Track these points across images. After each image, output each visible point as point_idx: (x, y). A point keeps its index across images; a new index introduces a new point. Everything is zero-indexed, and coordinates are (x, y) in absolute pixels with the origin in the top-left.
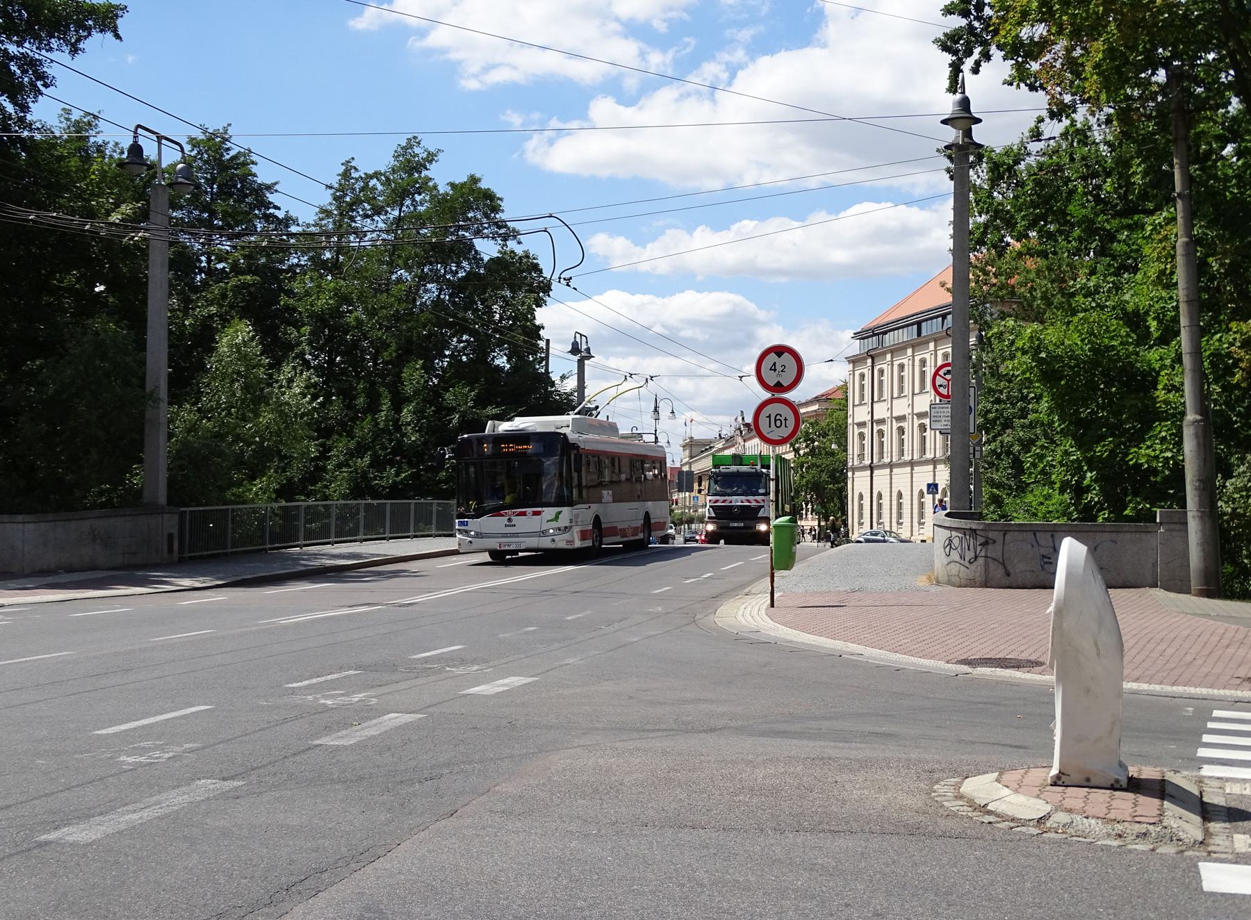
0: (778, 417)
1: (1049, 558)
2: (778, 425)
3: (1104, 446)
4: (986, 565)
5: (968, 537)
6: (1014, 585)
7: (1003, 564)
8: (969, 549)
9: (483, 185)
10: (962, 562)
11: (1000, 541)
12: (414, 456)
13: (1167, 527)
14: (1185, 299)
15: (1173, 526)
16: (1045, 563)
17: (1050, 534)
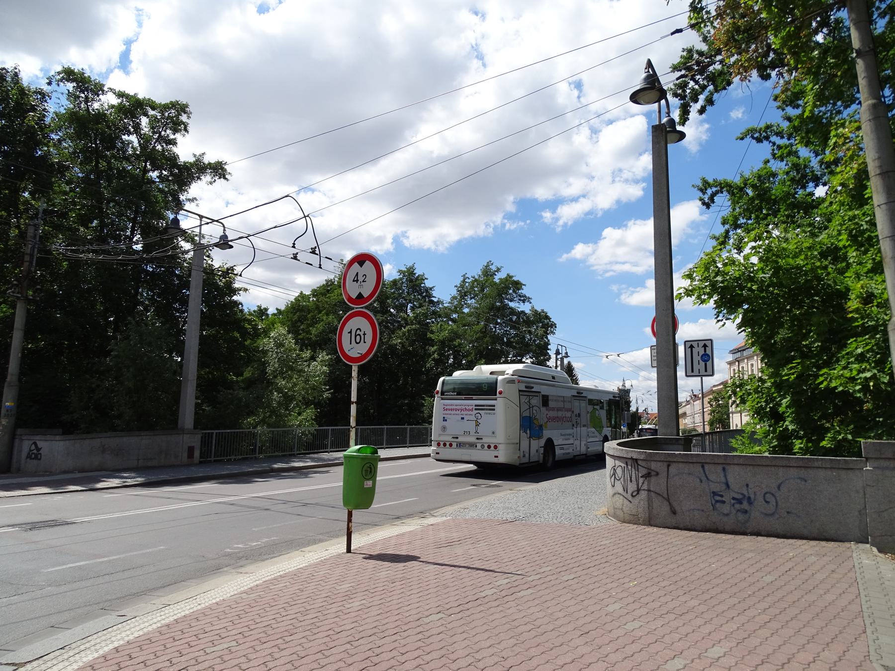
0: (358, 332)
1: (722, 496)
2: (358, 341)
3: (791, 368)
4: (650, 500)
5: (630, 467)
6: (681, 526)
7: (668, 500)
9: (515, 279)
10: (625, 494)
11: (663, 474)
13: (876, 464)
14: (878, 172)
15: (885, 463)
16: (717, 501)
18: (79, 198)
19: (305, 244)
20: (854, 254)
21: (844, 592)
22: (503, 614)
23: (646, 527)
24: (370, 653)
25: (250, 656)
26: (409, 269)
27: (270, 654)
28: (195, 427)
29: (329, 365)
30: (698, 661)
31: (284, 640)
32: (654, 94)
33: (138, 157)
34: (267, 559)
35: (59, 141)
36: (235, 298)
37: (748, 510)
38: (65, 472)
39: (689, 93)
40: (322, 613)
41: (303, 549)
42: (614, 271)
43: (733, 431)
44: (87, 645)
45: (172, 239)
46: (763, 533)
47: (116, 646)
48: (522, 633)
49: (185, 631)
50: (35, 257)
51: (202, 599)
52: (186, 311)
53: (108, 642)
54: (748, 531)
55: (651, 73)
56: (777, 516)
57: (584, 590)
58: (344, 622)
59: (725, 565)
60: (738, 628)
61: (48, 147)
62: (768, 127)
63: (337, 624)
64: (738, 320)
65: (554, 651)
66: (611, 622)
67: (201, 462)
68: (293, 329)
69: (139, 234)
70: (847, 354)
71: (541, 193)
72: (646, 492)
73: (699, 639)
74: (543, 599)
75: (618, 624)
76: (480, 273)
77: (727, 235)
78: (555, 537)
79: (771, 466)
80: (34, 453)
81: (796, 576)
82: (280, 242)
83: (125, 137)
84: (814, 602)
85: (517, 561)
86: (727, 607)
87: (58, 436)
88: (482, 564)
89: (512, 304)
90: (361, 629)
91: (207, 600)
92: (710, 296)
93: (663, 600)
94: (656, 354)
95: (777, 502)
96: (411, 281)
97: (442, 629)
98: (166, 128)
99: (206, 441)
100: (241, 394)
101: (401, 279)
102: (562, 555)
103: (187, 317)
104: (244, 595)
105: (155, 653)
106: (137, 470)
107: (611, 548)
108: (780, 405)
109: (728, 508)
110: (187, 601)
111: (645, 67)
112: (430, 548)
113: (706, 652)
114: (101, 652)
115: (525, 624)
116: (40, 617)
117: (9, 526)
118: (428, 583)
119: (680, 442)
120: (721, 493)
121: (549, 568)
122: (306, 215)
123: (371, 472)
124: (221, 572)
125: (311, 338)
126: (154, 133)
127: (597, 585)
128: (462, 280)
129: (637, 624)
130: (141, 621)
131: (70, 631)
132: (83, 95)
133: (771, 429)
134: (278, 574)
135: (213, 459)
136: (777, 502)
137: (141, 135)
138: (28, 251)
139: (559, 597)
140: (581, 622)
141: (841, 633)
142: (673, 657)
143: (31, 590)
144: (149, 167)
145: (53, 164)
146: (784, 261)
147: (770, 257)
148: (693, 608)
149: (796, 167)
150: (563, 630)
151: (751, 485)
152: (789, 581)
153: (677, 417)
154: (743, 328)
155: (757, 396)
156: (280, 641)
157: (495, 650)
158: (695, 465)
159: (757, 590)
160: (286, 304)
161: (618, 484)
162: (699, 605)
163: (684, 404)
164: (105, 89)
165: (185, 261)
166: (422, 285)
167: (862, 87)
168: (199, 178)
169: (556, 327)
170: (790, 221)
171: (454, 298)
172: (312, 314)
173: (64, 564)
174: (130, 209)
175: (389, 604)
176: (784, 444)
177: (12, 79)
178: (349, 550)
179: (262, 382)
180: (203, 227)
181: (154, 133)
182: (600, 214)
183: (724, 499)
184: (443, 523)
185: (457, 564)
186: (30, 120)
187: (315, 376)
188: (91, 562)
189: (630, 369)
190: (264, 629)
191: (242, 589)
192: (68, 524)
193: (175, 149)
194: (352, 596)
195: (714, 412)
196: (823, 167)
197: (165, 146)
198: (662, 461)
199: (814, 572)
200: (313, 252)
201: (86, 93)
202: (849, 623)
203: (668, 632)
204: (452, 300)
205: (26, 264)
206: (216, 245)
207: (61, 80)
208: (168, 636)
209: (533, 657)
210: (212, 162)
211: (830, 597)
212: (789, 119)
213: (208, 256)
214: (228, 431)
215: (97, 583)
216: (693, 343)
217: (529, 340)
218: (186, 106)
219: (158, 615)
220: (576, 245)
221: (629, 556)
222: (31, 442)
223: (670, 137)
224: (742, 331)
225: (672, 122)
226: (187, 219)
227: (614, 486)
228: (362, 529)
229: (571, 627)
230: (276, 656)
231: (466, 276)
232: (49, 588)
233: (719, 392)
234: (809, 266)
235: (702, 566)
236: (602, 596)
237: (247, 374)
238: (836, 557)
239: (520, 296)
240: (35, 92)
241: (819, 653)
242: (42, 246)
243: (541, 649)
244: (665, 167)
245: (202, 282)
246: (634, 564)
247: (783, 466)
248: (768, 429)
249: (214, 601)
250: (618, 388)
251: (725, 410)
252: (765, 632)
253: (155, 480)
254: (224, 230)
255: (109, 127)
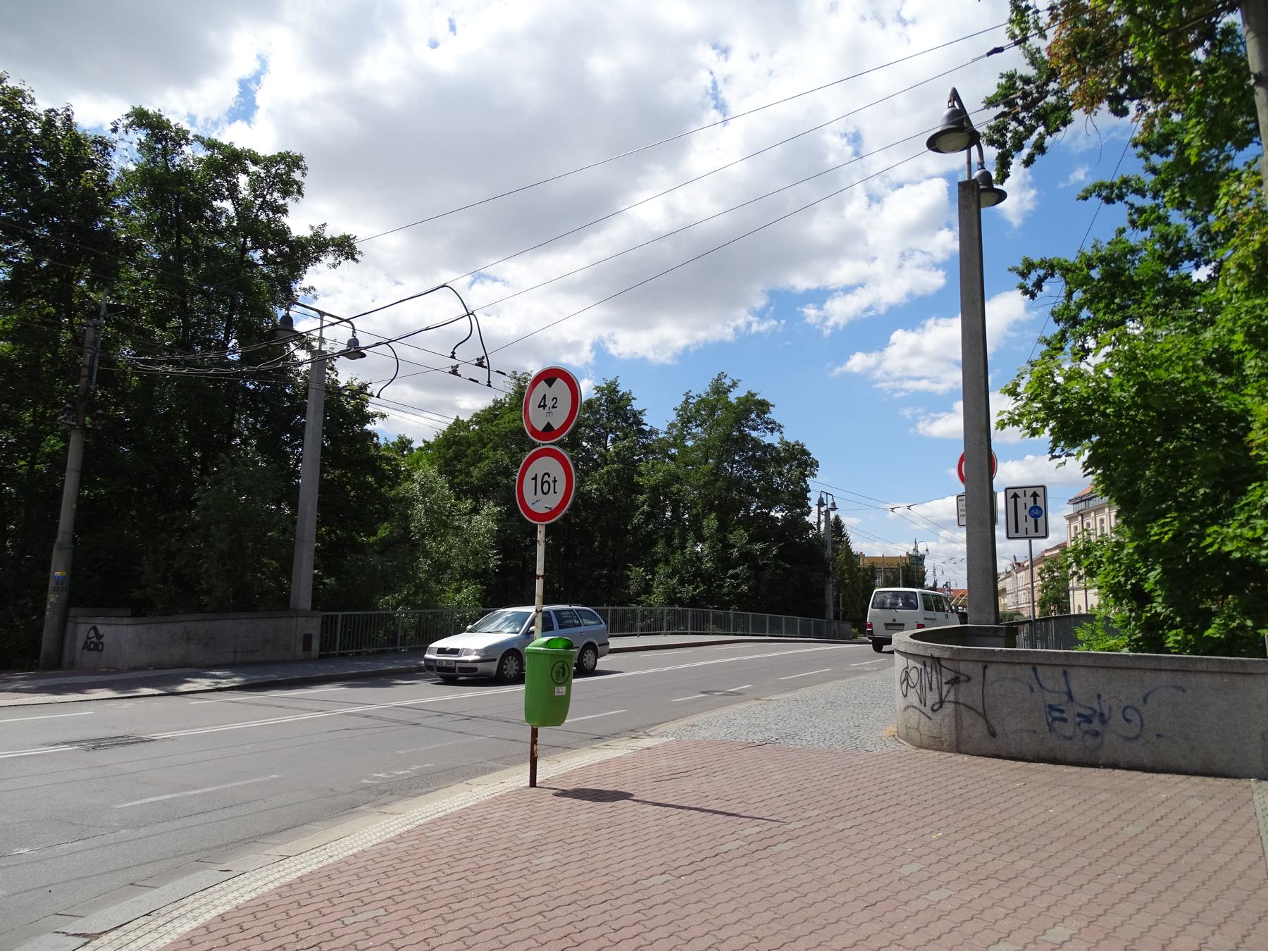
0: (546, 478)
1: (1062, 711)
2: (545, 491)
3: (1164, 525)
4: (958, 717)
5: (929, 669)
6: (1004, 753)
8: (931, 689)
9: (759, 397)
10: (922, 707)
11: (977, 679)
12: (707, 578)
16: (1055, 719)
17: (1060, 670)
18: (153, 289)
19: (469, 353)
20: (1253, 363)
21: (1241, 852)
22: (753, 877)
23: (952, 754)
24: (570, 929)
25: (405, 930)
26: (609, 386)
27: (432, 928)
28: (313, 608)
29: (497, 520)
30: (1033, 946)
31: (450, 908)
32: (962, 138)
33: (235, 231)
34: (420, 794)
35: (128, 210)
36: (368, 427)
37: (1101, 731)
38: (135, 669)
39: (1010, 138)
40: (501, 872)
41: (469, 781)
42: (907, 391)
43: (1075, 616)
44: (182, 911)
45: (282, 345)
46: (1122, 765)
47: (221, 912)
48: (781, 904)
49: (314, 893)
50: (96, 370)
51: (333, 849)
52: (301, 445)
53: (210, 907)
54: (1101, 762)
55: (958, 107)
56: (1142, 741)
57: (867, 844)
58: (532, 884)
59: (1068, 810)
60: (1089, 901)
61: (112, 217)
62: (1125, 182)
63: (522, 887)
64: (1084, 458)
65: (828, 928)
66: (907, 889)
67: (321, 657)
68: (447, 468)
69: (236, 338)
70: (1247, 504)
71: (800, 281)
72: (953, 705)
73: (1034, 915)
74: (810, 855)
75: (917, 893)
76: (708, 390)
77: (1063, 337)
78: (823, 768)
79: (1133, 669)
80: (93, 642)
81: (1172, 827)
82: (433, 351)
83: (217, 204)
84: (1197, 864)
85: (771, 801)
86: (1073, 870)
87: (126, 619)
88: (722, 804)
89: (754, 434)
90: (556, 894)
91: (340, 851)
92: (1045, 422)
93: (980, 859)
94: (964, 508)
95: (1142, 721)
96: (612, 401)
97: (669, 896)
98: (273, 191)
99: (328, 624)
100: (373, 560)
101: (598, 399)
102: (833, 794)
103: (301, 454)
104: (391, 845)
105: (274, 923)
106: (233, 666)
107: (903, 785)
108: (1145, 580)
109: (1071, 728)
110: (313, 851)
111: (948, 99)
112: (647, 781)
113: (1044, 934)
114: (201, 921)
115: (786, 891)
116: (114, 871)
117: (64, 743)
118: (646, 831)
119: (1000, 633)
120: (1061, 708)
121: (816, 812)
122: (470, 312)
123: (564, 674)
124: (354, 812)
125: (471, 482)
126: (256, 197)
127: (886, 837)
128: (684, 400)
129: (944, 893)
130: (252, 879)
131: (157, 890)
132: (160, 146)
133: (1133, 614)
134: (437, 816)
135: (337, 652)
136: (1142, 721)
137: (239, 200)
138: (87, 362)
139: (832, 853)
140: (865, 889)
141: (1237, 909)
142: (996, 940)
143: (101, 833)
144: (249, 244)
145: (118, 242)
146: (1152, 374)
147: (1131, 363)
148: (1024, 871)
149: (1164, 239)
150: (840, 899)
151: (1104, 697)
152: (1161, 835)
153: (996, 594)
154: (1090, 470)
155: (1111, 567)
156: (445, 909)
157: (745, 927)
158: (1024, 666)
159: (1115, 846)
160: (436, 434)
161: (912, 692)
162: (1032, 867)
163: (1002, 577)
164: (190, 137)
165: (299, 374)
166: (628, 408)
167: (1264, 128)
168: (317, 259)
169: (818, 466)
170: (1160, 313)
171: (672, 425)
172: (473, 448)
173: (142, 798)
174: (224, 302)
175: (593, 860)
176: (1152, 636)
177: (64, 124)
178: (533, 783)
179: (404, 544)
180: (324, 330)
181: (256, 197)
182: (882, 310)
183: (1065, 716)
184: (664, 745)
185: (686, 805)
186: (87, 180)
187: (477, 535)
188: (178, 795)
189: (926, 526)
190: (422, 893)
191: (388, 836)
192: (144, 741)
193: (284, 219)
194: (540, 848)
195: (1046, 587)
196: (1204, 238)
197: (271, 215)
198: (977, 661)
199: (1197, 822)
200: (480, 364)
201: (164, 143)
202: (1249, 896)
203: (989, 905)
204: (669, 429)
205: (84, 380)
206: (343, 353)
207: (130, 126)
208: (291, 900)
209: (798, 938)
210: (336, 236)
211: (1220, 858)
212: (1154, 171)
213: (331, 369)
214: (359, 613)
215: (189, 825)
216: (1018, 491)
217: (778, 486)
218: (300, 158)
219: (275, 870)
220: (854, 354)
221: (929, 796)
222: (89, 626)
223: (985, 197)
224: (1089, 474)
225: (987, 175)
226: (306, 319)
227: (906, 696)
228: (550, 754)
229: (849, 896)
230: (441, 929)
231: (690, 394)
232: (124, 831)
233: (1054, 559)
234: (1190, 382)
235: (1035, 811)
236: (893, 853)
237: (383, 531)
238: (1229, 800)
239: (767, 423)
240: (93, 142)
241: (1206, 939)
242: (105, 356)
243: (809, 927)
244: (977, 241)
245: (323, 406)
246: (937, 808)
247: (1151, 669)
248: (1128, 614)
249: (351, 852)
250: (907, 553)
251: (1063, 585)
252: (1127, 908)
253: (259, 681)
254: (354, 332)
255: (195, 191)
